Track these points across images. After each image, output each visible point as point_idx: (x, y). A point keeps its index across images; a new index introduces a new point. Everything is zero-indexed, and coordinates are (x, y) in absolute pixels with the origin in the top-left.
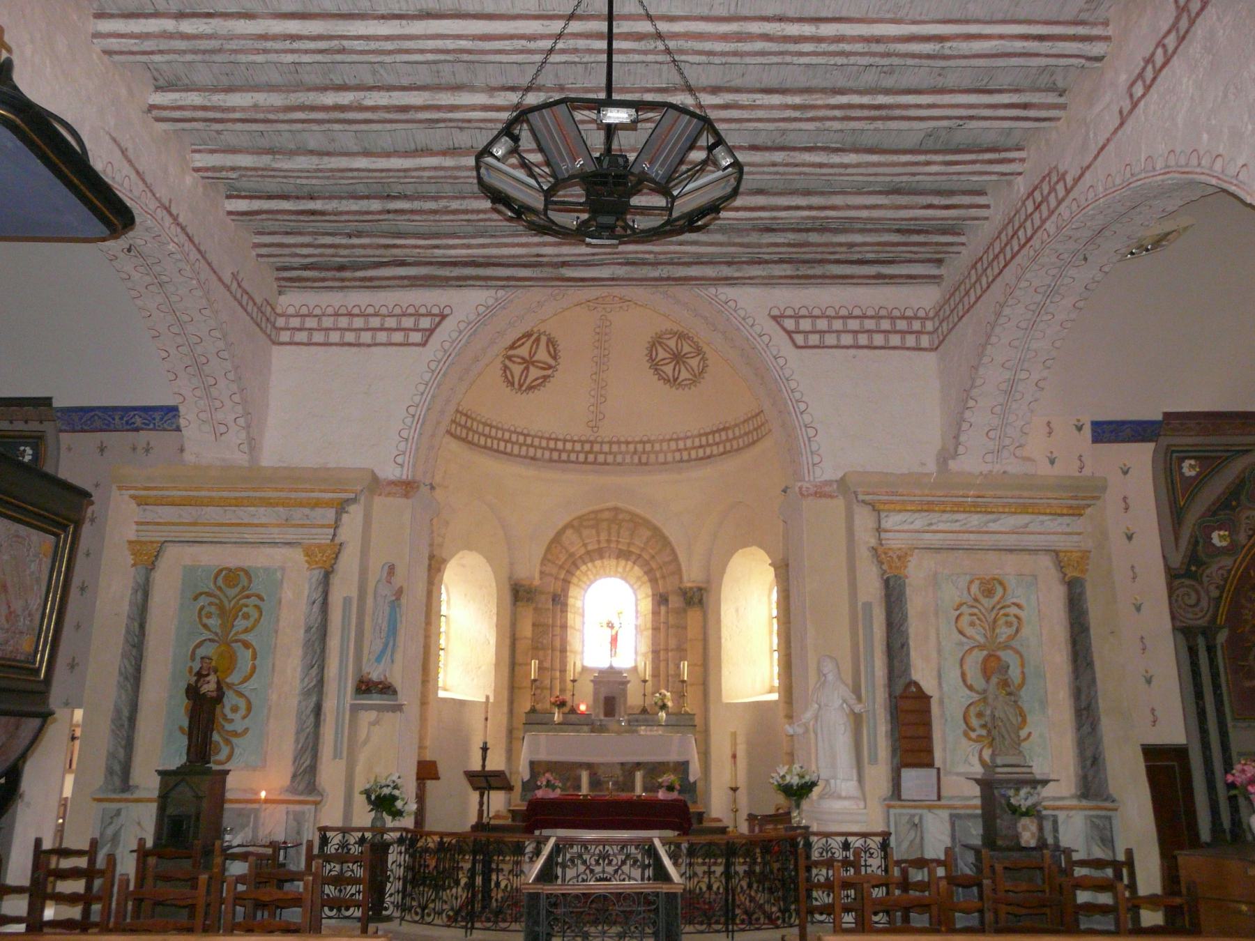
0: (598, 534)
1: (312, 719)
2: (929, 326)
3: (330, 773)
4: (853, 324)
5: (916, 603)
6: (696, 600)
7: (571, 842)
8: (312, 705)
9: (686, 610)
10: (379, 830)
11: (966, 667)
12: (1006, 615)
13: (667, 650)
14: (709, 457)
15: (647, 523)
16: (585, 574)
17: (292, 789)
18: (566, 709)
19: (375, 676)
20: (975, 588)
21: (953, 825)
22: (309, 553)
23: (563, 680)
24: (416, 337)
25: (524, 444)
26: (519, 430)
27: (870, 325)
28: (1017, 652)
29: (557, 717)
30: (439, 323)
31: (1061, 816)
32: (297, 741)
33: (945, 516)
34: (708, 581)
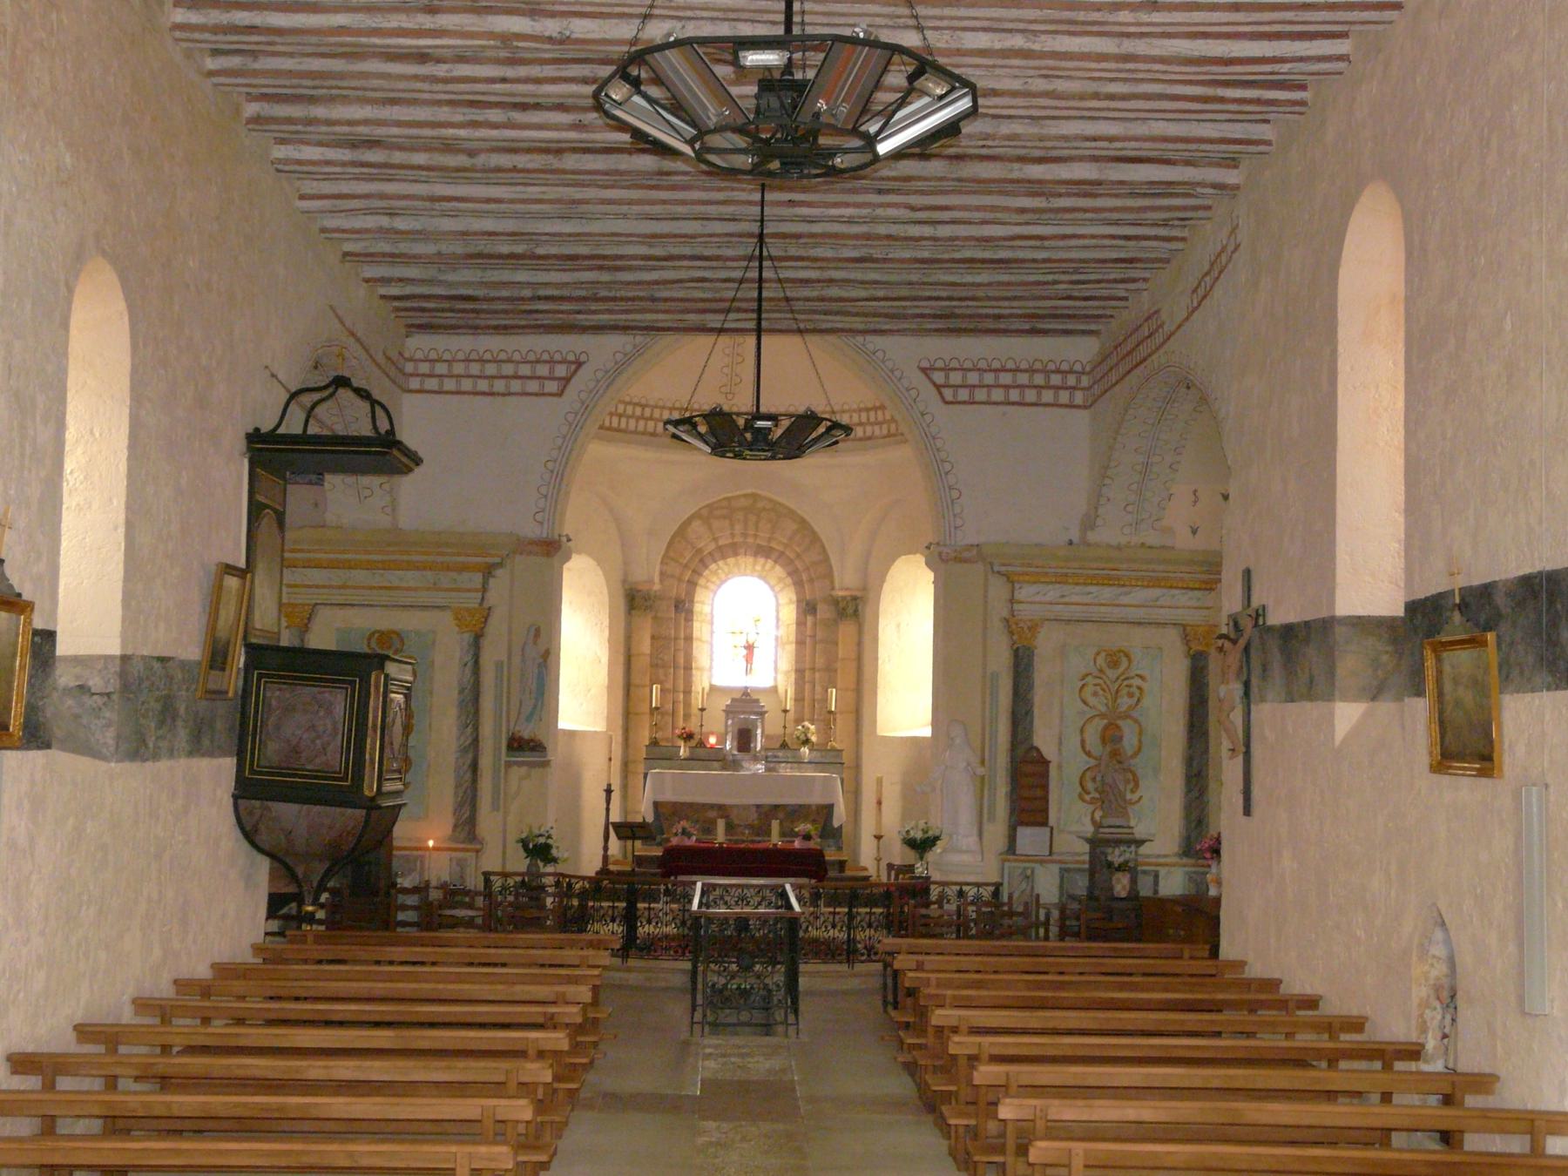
0: (732, 526)
1: (468, 775)
2: (1085, 381)
3: (488, 823)
4: (1006, 378)
5: (1043, 672)
6: (850, 611)
7: (714, 886)
8: (469, 762)
9: (836, 623)
10: (534, 874)
11: (1087, 735)
12: (1129, 686)
13: (813, 669)
14: (870, 438)
15: (791, 514)
16: (715, 573)
17: (452, 839)
18: (693, 743)
19: (526, 735)
20: (1101, 661)
21: (1062, 878)
22: (458, 619)
23: (687, 704)
24: (552, 386)
25: (642, 417)
26: (636, 400)
27: (1023, 379)
28: (1136, 721)
29: (683, 752)
30: (576, 371)
31: (1162, 871)
32: (456, 794)
33: (1078, 588)
34: (864, 589)
